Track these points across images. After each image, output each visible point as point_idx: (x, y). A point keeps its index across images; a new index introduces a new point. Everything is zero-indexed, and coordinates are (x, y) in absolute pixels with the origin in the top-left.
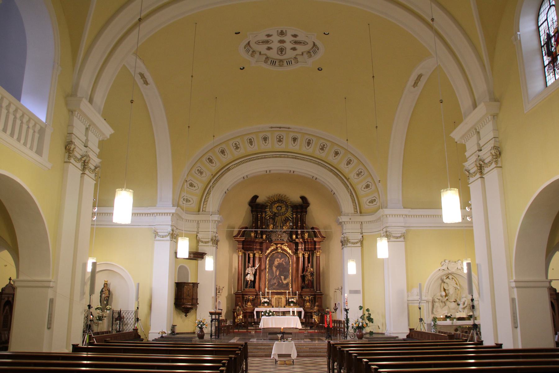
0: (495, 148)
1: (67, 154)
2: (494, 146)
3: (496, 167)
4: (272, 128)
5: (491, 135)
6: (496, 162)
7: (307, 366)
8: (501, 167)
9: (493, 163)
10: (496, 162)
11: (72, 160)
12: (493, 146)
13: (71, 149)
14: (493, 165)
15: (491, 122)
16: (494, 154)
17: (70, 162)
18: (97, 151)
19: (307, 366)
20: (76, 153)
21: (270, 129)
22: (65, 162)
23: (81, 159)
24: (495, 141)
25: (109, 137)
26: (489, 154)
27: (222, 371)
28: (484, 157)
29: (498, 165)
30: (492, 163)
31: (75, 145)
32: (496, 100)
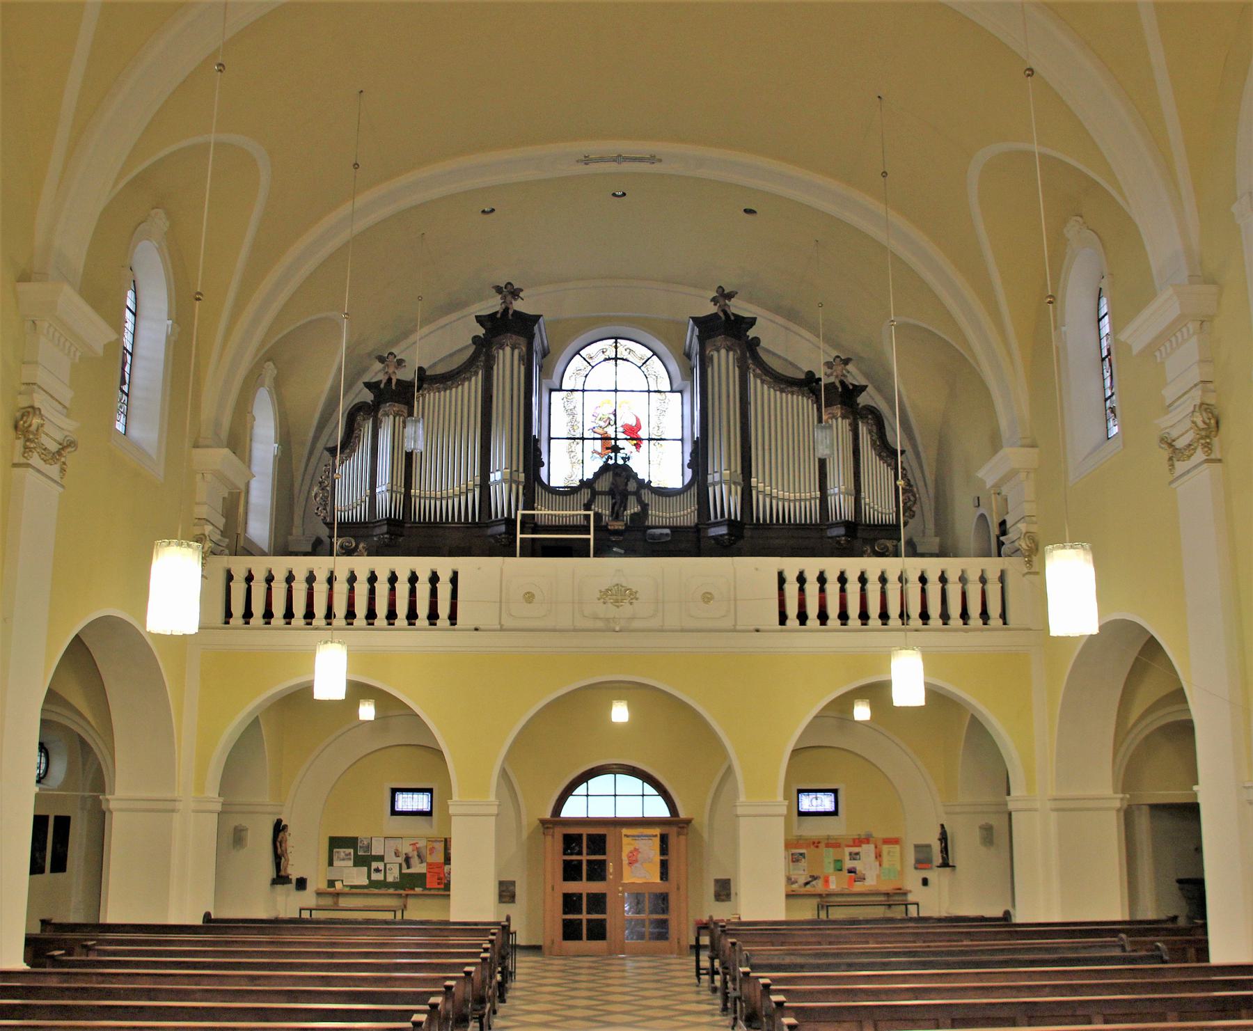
0: (1204, 407)
1: (19, 443)
2: (1202, 404)
3: (1207, 461)
4: (587, 160)
5: (1195, 375)
6: (1208, 447)
7: (645, 998)
8: (1220, 461)
9: (1199, 450)
10: (1208, 447)
11: (35, 460)
12: (1198, 402)
13: (33, 428)
14: (1199, 455)
15: (1194, 340)
16: (1201, 425)
17: (28, 465)
18: (67, 395)
19: (645, 998)
20: (44, 440)
21: (582, 169)
22: (15, 465)
23: (59, 453)
24: (1204, 391)
25: (100, 352)
26: (1188, 424)
27: (417, 1024)
28: (1174, 433)
29: (1213, 456)
30: (1195, 449)
31: (42, 416)
32: (1210, 280)
